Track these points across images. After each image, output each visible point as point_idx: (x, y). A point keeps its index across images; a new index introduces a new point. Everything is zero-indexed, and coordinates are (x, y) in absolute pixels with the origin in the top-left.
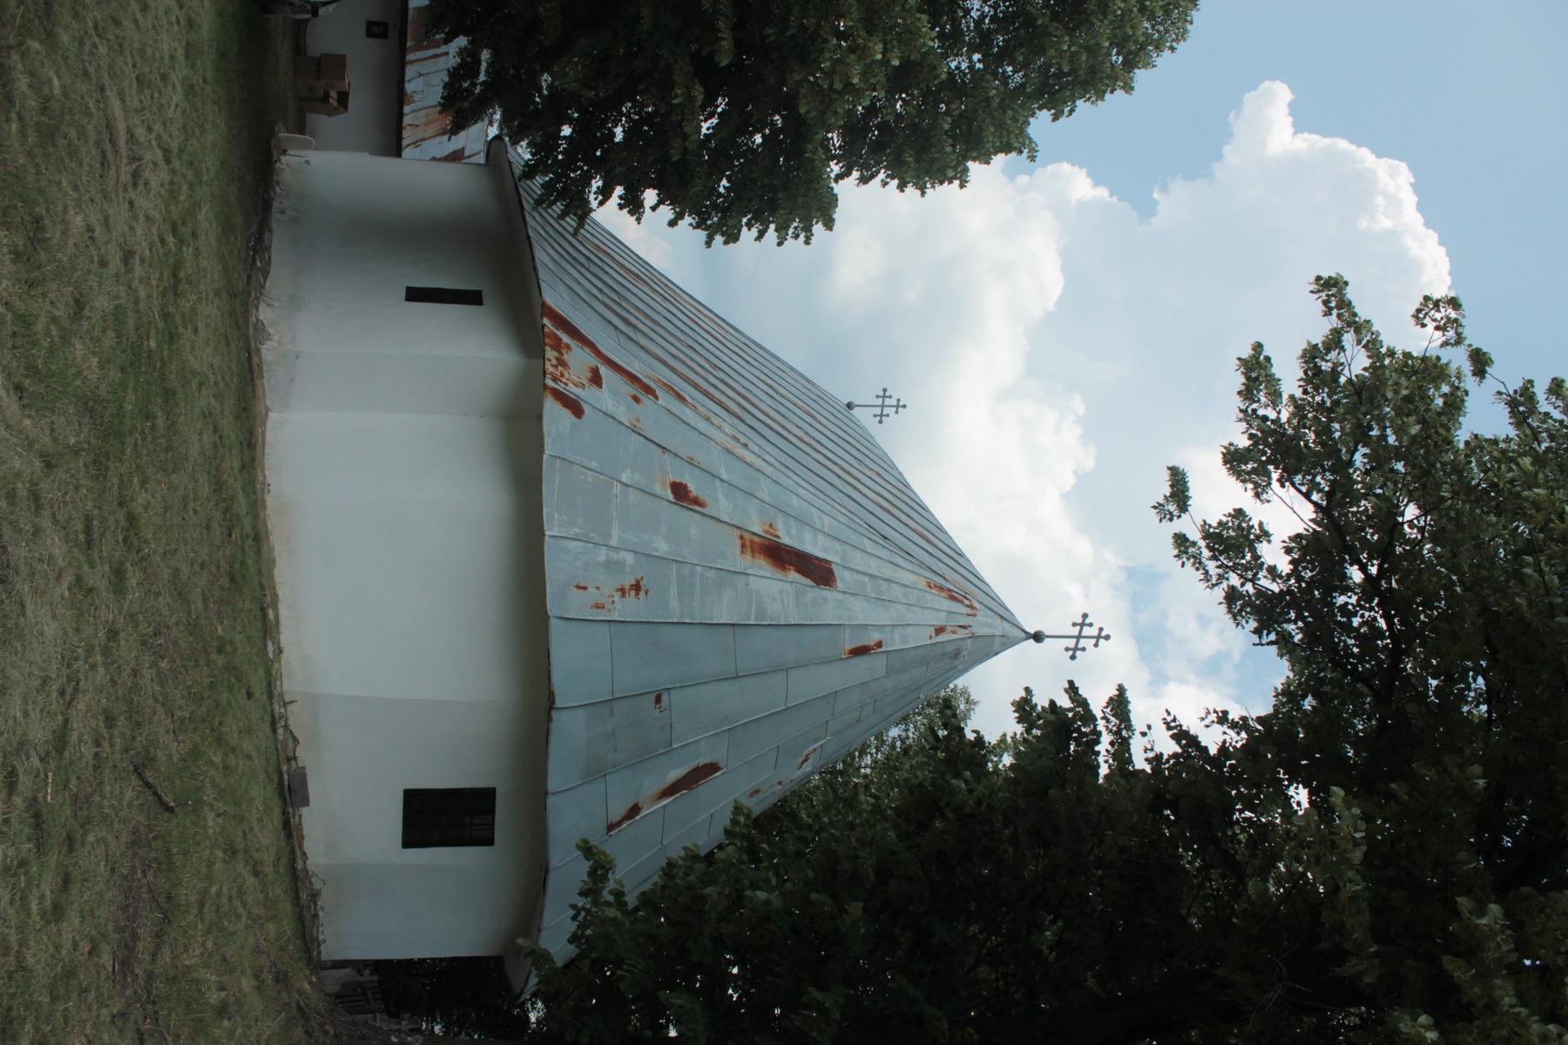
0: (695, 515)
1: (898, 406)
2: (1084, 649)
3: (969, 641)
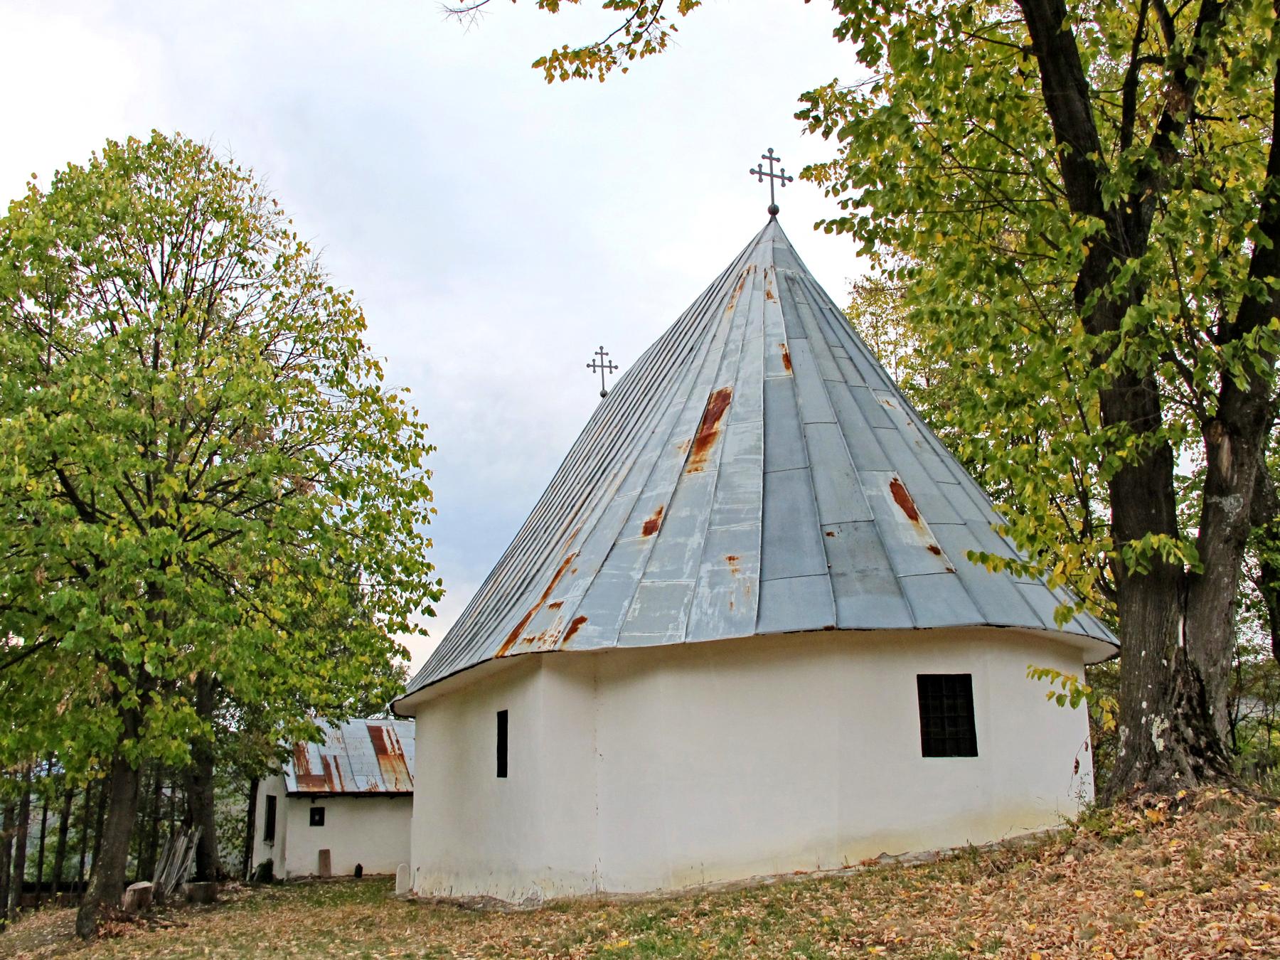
0: (670, 513)
2: (783, 171)
3: (778, 269)
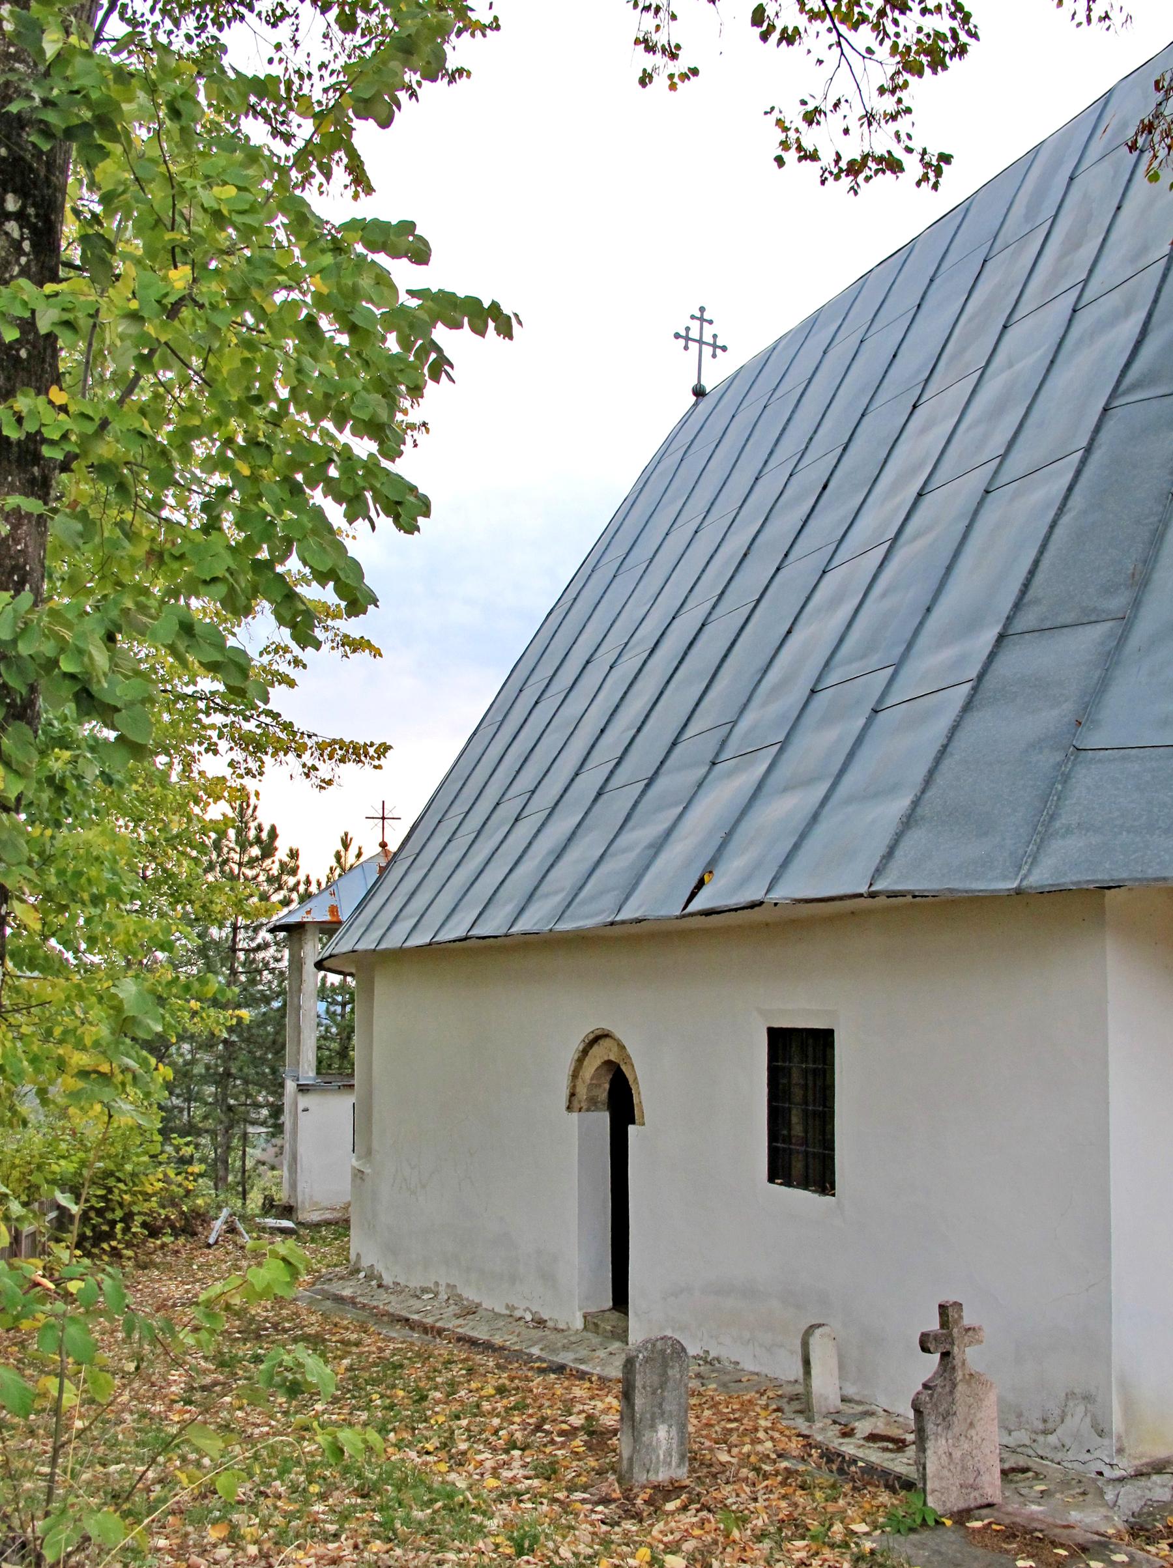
1: (702, 320)
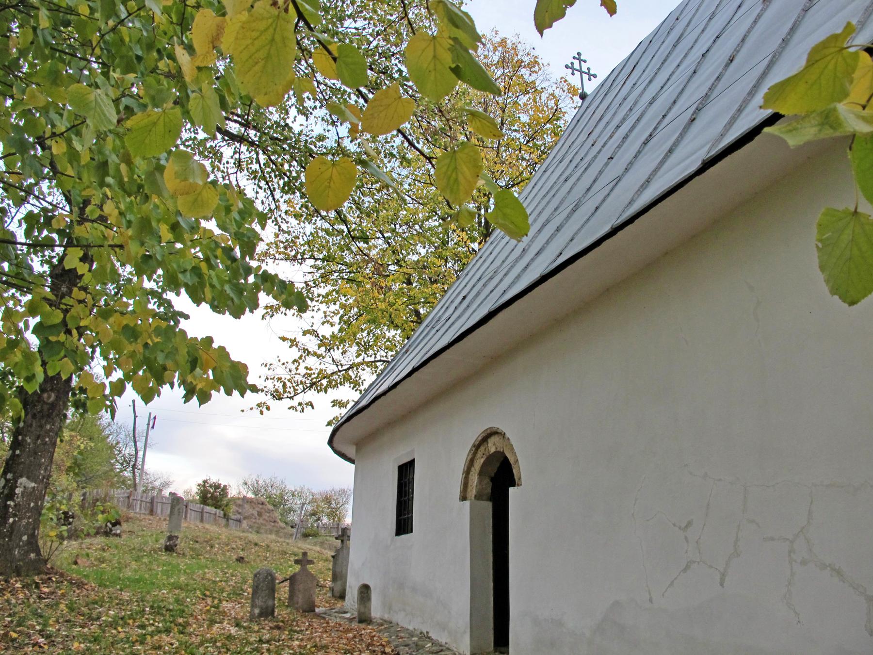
1: (580, 60)
